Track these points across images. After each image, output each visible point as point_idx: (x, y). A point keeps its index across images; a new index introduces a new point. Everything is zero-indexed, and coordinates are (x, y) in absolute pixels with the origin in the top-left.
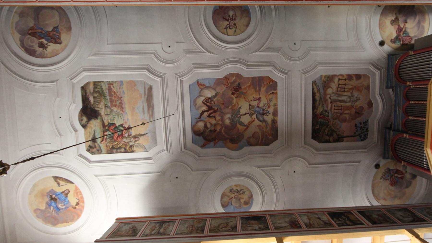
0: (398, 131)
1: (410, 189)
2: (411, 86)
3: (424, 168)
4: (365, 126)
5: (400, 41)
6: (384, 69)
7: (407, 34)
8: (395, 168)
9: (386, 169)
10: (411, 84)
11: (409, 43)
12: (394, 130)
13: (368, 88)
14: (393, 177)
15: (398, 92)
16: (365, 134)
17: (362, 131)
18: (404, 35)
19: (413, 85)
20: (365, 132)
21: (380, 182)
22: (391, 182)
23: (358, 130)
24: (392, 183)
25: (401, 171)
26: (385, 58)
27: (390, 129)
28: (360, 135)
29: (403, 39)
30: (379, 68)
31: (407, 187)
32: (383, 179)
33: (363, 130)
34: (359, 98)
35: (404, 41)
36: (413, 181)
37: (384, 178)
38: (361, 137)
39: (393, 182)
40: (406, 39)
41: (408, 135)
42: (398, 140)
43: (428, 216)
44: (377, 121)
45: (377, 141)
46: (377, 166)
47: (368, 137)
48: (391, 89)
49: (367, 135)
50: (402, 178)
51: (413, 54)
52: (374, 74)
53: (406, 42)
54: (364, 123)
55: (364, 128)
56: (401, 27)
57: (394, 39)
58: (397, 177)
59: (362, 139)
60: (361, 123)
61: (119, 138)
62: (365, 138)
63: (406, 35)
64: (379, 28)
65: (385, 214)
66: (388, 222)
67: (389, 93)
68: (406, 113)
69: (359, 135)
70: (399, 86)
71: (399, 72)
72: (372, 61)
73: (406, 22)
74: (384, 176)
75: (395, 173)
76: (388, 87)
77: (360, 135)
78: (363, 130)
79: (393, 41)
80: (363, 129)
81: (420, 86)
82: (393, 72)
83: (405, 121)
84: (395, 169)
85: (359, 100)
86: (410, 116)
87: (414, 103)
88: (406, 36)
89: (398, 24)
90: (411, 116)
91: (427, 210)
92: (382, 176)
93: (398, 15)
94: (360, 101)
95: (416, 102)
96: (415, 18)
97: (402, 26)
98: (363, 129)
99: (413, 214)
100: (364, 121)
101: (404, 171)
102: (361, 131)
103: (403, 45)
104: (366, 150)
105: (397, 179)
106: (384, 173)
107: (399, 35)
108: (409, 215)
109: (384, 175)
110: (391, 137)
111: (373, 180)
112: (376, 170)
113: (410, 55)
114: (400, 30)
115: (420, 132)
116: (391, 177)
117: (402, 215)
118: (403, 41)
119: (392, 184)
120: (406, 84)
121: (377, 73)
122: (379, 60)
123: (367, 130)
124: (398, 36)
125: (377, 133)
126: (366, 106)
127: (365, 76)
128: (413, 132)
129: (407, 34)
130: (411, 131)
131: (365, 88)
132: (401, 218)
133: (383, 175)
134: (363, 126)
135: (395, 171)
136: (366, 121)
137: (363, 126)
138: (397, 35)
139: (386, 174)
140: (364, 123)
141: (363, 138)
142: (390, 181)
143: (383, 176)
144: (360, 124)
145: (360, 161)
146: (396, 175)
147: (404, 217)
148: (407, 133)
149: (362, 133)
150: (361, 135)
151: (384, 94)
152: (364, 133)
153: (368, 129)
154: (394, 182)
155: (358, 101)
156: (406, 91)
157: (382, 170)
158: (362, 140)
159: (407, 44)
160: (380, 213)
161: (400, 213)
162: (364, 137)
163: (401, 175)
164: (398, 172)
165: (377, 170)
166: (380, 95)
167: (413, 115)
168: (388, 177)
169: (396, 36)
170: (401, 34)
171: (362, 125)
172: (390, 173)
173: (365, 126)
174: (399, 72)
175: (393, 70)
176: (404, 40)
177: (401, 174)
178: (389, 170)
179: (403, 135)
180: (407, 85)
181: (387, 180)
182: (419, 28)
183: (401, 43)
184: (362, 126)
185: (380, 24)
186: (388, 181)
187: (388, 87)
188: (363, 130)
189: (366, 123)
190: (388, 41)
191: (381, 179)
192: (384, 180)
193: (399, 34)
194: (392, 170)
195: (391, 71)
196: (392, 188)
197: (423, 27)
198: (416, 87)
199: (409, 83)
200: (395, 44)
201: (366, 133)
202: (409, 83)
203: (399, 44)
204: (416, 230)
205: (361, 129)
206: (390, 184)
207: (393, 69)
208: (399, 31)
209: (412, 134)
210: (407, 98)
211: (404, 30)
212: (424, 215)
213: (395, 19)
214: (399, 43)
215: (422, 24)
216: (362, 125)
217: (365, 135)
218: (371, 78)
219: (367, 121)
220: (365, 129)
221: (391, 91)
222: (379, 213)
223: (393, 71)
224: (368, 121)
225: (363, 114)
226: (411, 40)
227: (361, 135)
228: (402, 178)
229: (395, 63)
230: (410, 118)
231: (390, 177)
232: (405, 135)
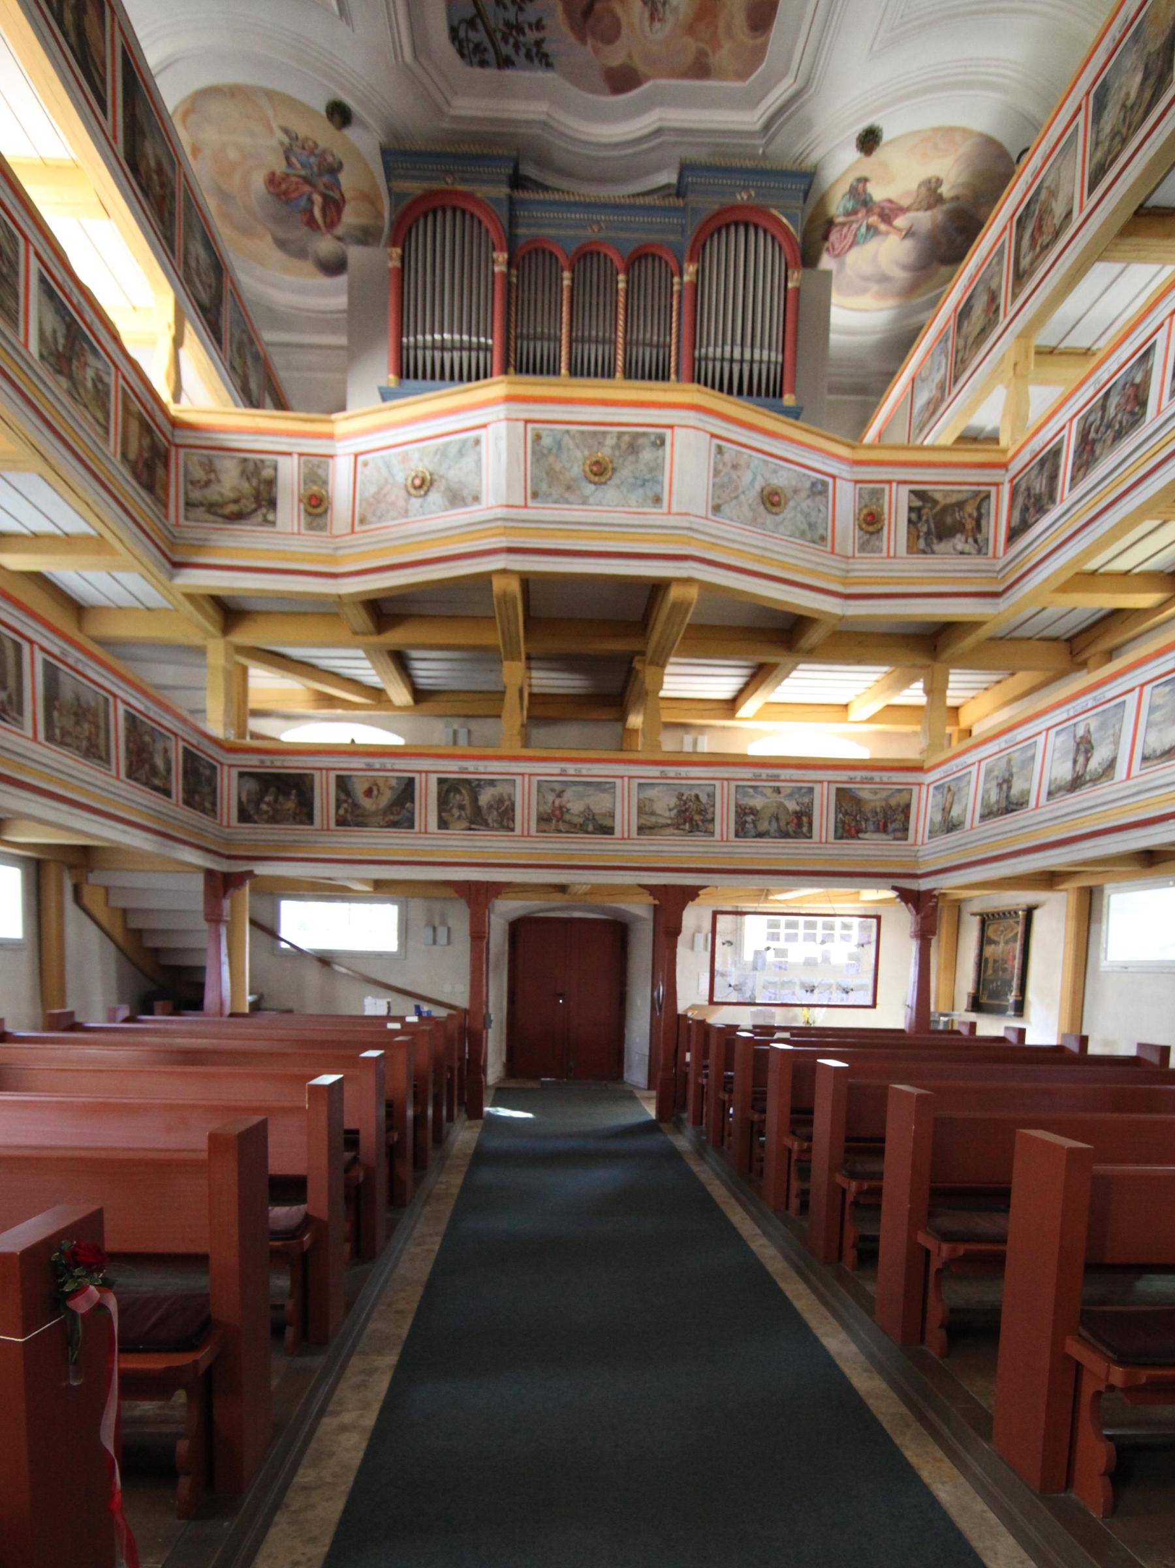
0: (513, 221)
1: (278, 255)
2: (681, 276)
3: (402, 336)
4: (523, 51)
5: (848, 214)
6: (761, 151)
7: (861, 241)
8: (347, 195)
9: (333, 156)
10: (686, 278)
11: (826, 245)
12: (512, 202)
13: (701, 69)
14: (307, 189)
15: (663, 220)
16: (485, 50)
17: (499, 36)
18: (863, 230)
19: (681, 283)
20: (497, 52)
21: (271, 130)
22: (284, 179)
23: (505, 8)
24: (280, 184)
25: (339, 218)
26: (805, 154)
27: (517, 181)
28: (478, 21)
29: (850, 226)
30: (773, 124)
31: (281, 244)
32: (286, 140)
33: (506, 42)
34: (660, 20)
35: (841, 230)
36: (308, 266)
37: (291, 145)
38: (471, 24)
39: (284, 186)
40: (845, 237)
41: (504, 268)
42: (467, 217)
43: (234, 349)
44: (544, 117)
45: (463, 113)
46: (340, 114)
47: (471, 65)
48: (674, 179)
49: (483, 64)
50: (311, 222)
51: (790, 285)
52: (753, 104)
53: (834, 236)
54: (539, 43)
55: (516, 46)
56: (896, 216)
57: (865, 190)
58: (311, 201)
59: (462, 34)
60: (539, 25)
61: (1128, 94)
62: (466, 52)
63: (859, 235)
64: (936, 130)
65: (173, 195)
66: (162, 220)
67: (657, 169)
68: (586, 256)
69: (480, 13)
70: (684, 221)
71: (737, 225)
72: (813, 90)
73: (909, 234)
74: (303, 148)
75: (325, 197)
76: (685, 168)
77: (478, 21)
78: (505, 40)
79: (861, 186)
80: (511, 41)
81: (674, 314)
82: (742, 199)
83: (551, 254)
84: (342, 195)
85: (652, 18)
86: (573, 271)
87: (617, 290)
88: (855, 235)
89: (915, 206)
90: (573, 280)
91: (245, 337)
92: (300, 136)
93: (945, 207)
94: (647, 23)
95: (622, 299)
96: (905, 267)
97: (900, 222)
98: (511, 41)
99: (218, 299)
100: (546, 48)
101: (340, 230)
102: (501, 26)
103: (830, 224)
104: (408, 57)
105: (303, 202)
106: (316, 145)
107: (869, 212)
108: (210, 286)
109: (306, 146)
110: (482, 191)
111: (269, 94)
112: (322, 109)
113: (790, 272)
114: (888, 213)
115: (520, 317)
116: (306, 180)
117: (201, 262)
118: (843, 224)
119: (272, 181)
120: (691, 260)
121: (751, 119)
122: (807, 126)
123: (505, 63)
124: (870, 205)
125: (488, 114)
126: (616, 56)
127: (757, 55)
128: (517, 287)
129: (861, 241)
130: (518, 278)
131: (701, 54)
132: (193, 264)
133: (307, 139)
134: (521, 39)
135: (336, 195)
136: (546, 56)
137: (521, 39)
138: (875, 203)
139: (312, 153)
140: (539, 43)
141: (468, 40)
142: (288, 175)
143: (299, 143)
144: (534, 20)
145: (347, 23)
146: (317, 199)
147: (199, 275)
148: (510, 263)
149: (490, 34)
150: (480, 27)
151: (660, 145)
152: (489, 46)
153: (508, 67)
154: (286, 193)
155: (647, 14)
156: (665, 256)
157: (324, 135)
158: (454, 32)
159: (826, 238)
160: (170, 174)
161: (203, 254)
162: (471, 46)
163: (325, 222)
164: (334, 206)
165: (324, 113)
166: (658, 132)
167: (576, 285)
168: (303, 166)
169: (871, 199)
170: (873, 219)
171: (527, 30)
172: (320, 175)
173: (523, 51)
174: (737, 225)
175: (750, 196)
176: (845, 230)
177: (328, 220)
178: (334, 170)
179: (502, 250)
180: (685, 265)
181: (288, 159)
182: (865, 278)
183: (838, 216)
184: (524, 34)
185: (951, 130)
186: (284, 162)
187: (685, 168)
188: (505, 40)
189: (540, 57)
190: (868, 166)
191: (286, 131)
192: (282, 144)
193: (877, 210)
194: (337, 184)
195: (745, 188)
196: (258, 181)
197: (864, 291)
198: (675, 297)
199: (691, 269)
200: (843, 197)
201: (490, 56)
202: (691, 269)
203: (837, 209)
204: (188, 329)
205: (507, 24)
206: (273, 174)
207: (753, 193)
208: (887, 211)
209: (509, 283)
210: (639, 257)
211: (883, 227)
212: (232, 335)
213: (940, 196)
214: (841, 210)
215: (875, 288)
216: (531, 36)
217: (478, 48)
218: (738, 84)
219: (546, 62)
220: (507, 50)
221: (668, 177)
222: (166, 166)
223: (745, 197)
224: (549, 65)
225: (582, 39)
226: (837, 252)
227: (480, 27)
228: (311, 222)
229: (776, 207)
230: (567, 275)
231: (303, 173)
232: (501, 257)
